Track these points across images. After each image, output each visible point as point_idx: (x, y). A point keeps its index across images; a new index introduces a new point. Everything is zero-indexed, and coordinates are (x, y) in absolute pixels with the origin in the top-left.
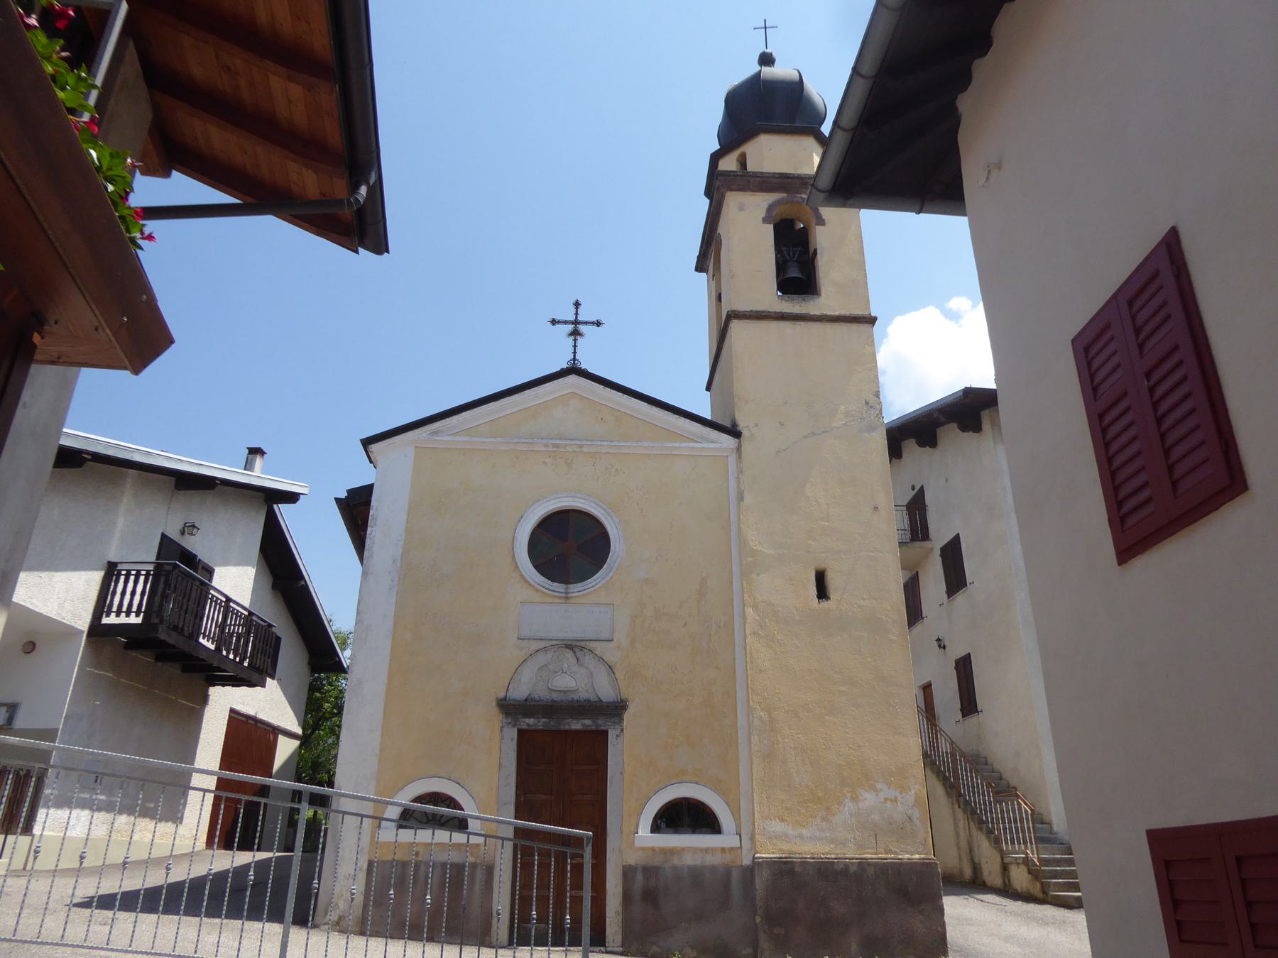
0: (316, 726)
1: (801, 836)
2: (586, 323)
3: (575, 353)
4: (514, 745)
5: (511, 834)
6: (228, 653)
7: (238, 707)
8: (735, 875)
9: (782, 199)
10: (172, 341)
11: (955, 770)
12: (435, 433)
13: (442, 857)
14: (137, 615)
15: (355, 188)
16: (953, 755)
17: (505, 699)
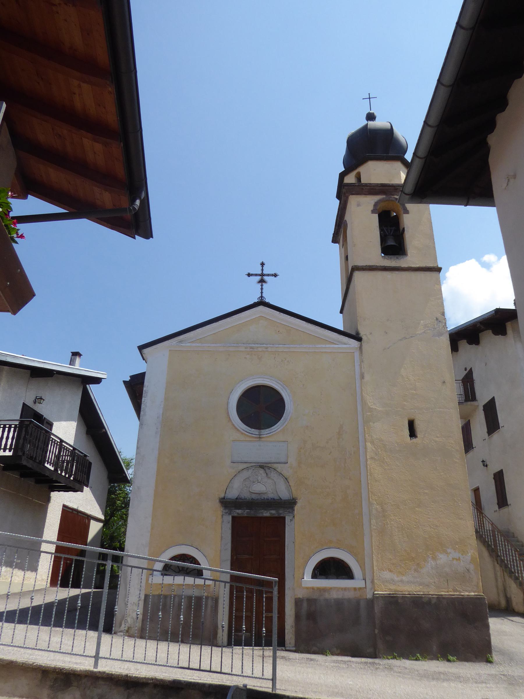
0: (112, 515)
1: (402, 581)
2: (268, 275)
3: (262, 293)
4: (229, 526)
5: (228, 580)
6: (62, 472)
7: (67, 504)
8: (363, 604)
9: (383, 198)
10: (34, 295)
11: (495, 541)
12: (181, 342)
13: (189, 592)
14: (10, 451)
15: (133, 201)
16: (493, 531)
17: (224, 498)
